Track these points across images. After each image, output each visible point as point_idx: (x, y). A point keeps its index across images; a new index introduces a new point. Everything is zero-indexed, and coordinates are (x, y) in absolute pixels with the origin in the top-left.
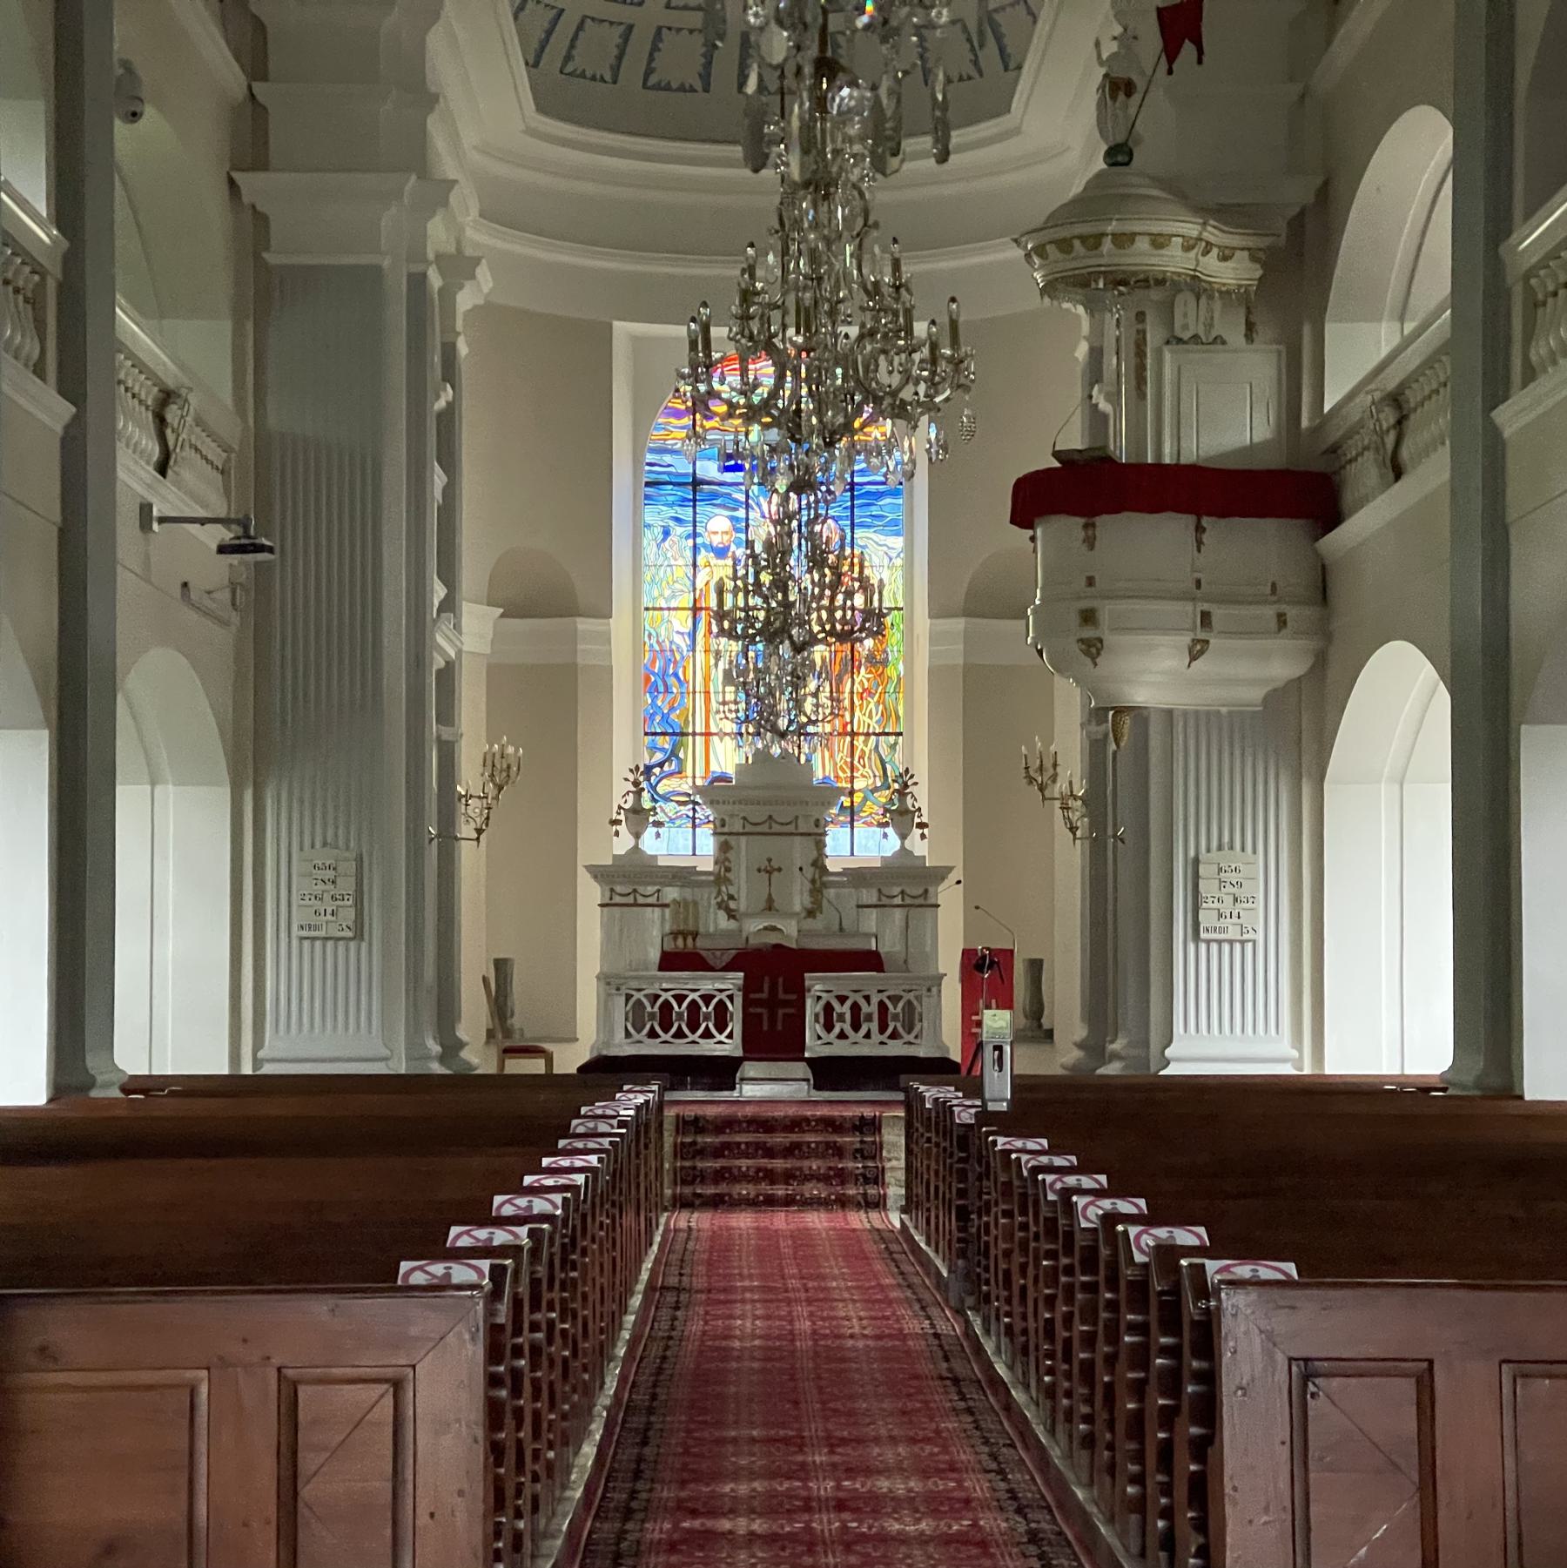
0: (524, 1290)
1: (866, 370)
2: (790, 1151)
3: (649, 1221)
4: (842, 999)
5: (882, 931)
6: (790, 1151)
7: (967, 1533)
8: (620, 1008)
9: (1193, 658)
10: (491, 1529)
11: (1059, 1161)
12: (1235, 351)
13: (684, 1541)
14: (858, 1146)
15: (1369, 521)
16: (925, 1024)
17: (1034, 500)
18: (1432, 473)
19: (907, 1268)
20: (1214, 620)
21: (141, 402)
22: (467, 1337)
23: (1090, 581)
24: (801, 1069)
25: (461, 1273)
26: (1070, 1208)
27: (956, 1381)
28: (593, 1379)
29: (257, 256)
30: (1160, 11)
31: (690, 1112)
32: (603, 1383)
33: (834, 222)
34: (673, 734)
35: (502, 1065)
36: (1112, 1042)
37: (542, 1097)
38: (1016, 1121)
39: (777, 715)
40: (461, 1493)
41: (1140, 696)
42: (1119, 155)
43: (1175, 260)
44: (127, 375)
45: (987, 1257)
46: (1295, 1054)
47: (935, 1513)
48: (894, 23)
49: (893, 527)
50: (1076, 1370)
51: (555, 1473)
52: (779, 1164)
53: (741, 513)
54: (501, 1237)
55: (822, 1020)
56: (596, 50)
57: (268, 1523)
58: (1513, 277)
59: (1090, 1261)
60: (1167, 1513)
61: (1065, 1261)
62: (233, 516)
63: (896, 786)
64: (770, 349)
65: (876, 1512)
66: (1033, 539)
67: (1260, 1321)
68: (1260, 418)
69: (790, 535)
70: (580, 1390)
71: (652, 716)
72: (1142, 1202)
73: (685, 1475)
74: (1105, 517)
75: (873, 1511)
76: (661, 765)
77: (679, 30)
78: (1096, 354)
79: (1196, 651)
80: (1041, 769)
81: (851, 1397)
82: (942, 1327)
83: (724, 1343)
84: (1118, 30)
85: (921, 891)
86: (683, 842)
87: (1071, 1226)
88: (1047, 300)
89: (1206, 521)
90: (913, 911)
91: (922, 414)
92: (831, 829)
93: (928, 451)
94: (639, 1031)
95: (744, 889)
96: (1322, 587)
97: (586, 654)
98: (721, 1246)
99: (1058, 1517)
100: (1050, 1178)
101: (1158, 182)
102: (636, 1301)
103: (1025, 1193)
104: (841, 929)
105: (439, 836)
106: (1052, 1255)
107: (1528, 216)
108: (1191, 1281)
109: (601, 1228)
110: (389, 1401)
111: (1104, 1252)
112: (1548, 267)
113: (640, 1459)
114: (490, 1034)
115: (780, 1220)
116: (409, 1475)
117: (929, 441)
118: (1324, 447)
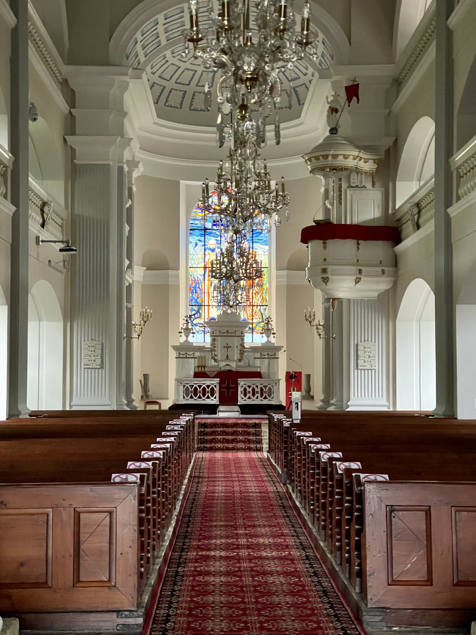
0: (150, 482)
1: (256, 199)
2: (233, 434)
3: (190, 456)
4: (249, 387)
5: (261, 365)
6: (233, 434)
7: (287, 556)
8: (181, 389)
9: (357, 283)
10: (140, 558)
11: (315, 440)
12: (369, 190)
13: (200, 559)
14: (254, 432)
15: (410, 242)
16: (275, 395)
17: (308, 235)
18: (429, 228)
19: (269, 470)
20: (363, 271)
21: (36, 206)
22: (132, 498)
23: (325, 260)
24: (237, 408)
25: (131, 478)
26: (319, 456)
27: (284, 507)
28: (172, 506)
29: (72, 162)
30: (346, 87)
31: (203, 421)
32: (175, 508)
33: (246, 154)
34: (198, 305)
35: (145, 407)
36: (332, 400)
37: (158, 418)
38: (301, 427)
39: (230, 301)
40: (130, 547)
41: (340, 294)
42: (334, 131)
43: (350, 163)
44: (32, 197)
45: (293, 468)
46: (388, 404)
47: (278, 550)
48: (263, 102)
49: (266, 243)
50: (320, 505)
51: (161, 538)
52: (230, 437)
53: (219, 238)
54: (143, 465)
55: (243, 393)
56: (175, 99)
57: (71, 556)
58: (453, 168)
59: (325, 472)
60: (349, 552)
61: (317, 471)
62: (64, 240)
63: (266, 322)
64: (227, 192)
65: (259, 550)
66: (307, 247)
67: (378, 493)
68: (377, 210)
69: (233, 246)
70: (168, 511)
71: (192, 300)
72: (341, 453)
73: (201, 537)
74: (330, 240)
75: (258, 549)
76: (194, 315)
77: (200, 93)
78: (327, 191)
79: (357, 281)
80: (310, 316)
81: (251, 512)
82: (280, 490)
83: (213, 494)
84: (333, 93)
85: (273, 353)
86: (201, 339)
87: (319, 460)
88: (312, 174)
89: (360, 242)
90: (271, 360)
91: (273, 212)
92: (246, 334)
93: (275, 224)
94: (187, 396)
95: (220, 354)
96: (395, 262)
97: (171, 281)
98: (212, 462)
99: (315, 551)
100: (312, 445)
101: (346, 139)
102: (186, 481)
103: (305, 448)
104: (249, 365)
105: (126, 337)
106: (313, 469)
107: (458, 149)
108: (356, 481)
109: (175, 460)
110: (108, 518)
111: (329, 469)
112: (464, 166)
113: (187, 532)
114: (142, 397)
115: (230, 455)
116: (114, 542)
117: (275, 221)
118: (396, 219)
